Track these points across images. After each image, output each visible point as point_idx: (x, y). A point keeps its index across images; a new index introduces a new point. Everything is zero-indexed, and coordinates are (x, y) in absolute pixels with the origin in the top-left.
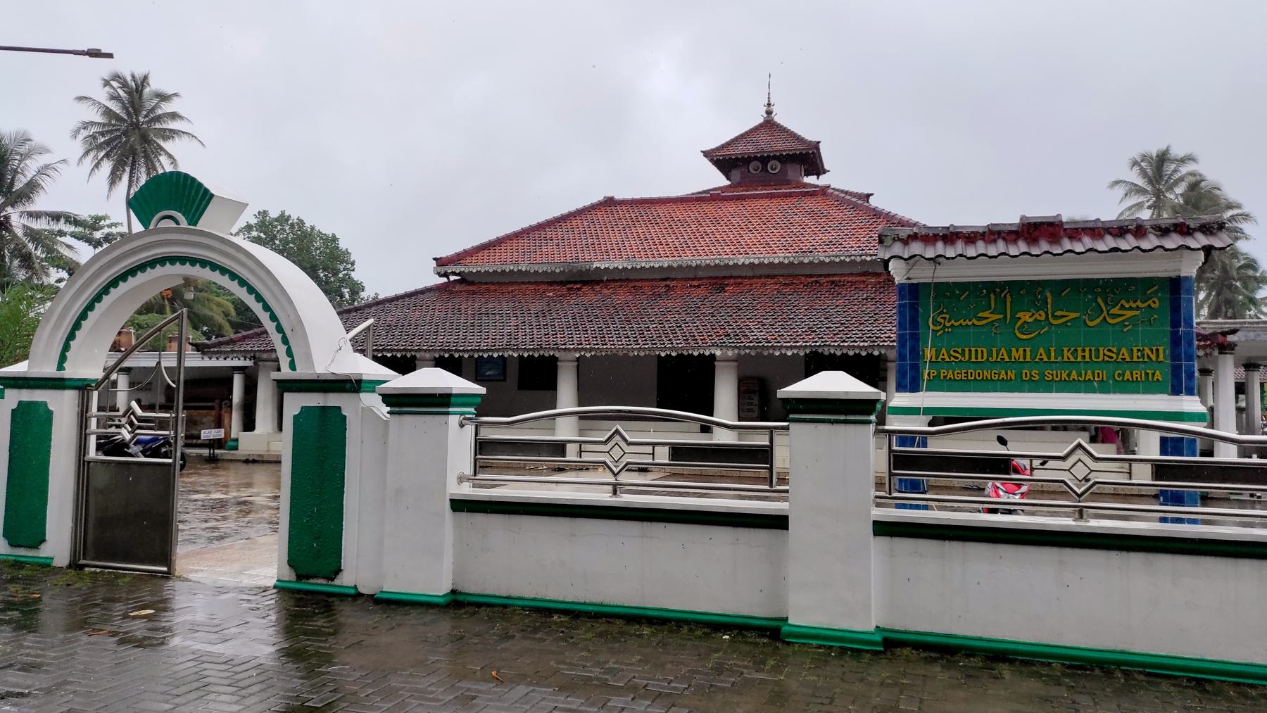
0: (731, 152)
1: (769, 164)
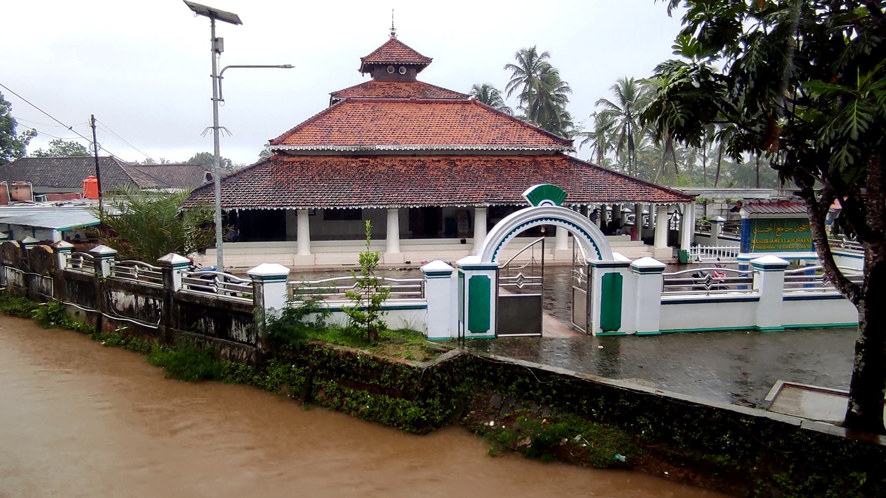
0: (372, 61)
1: (393, 70)
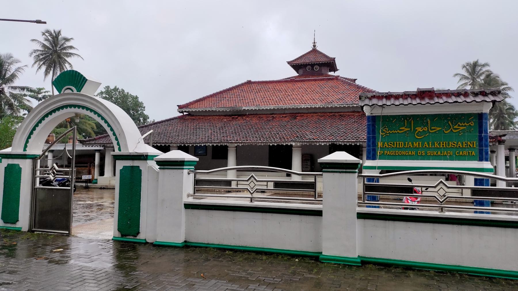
0: (299, 62)
1: (314, 67)
